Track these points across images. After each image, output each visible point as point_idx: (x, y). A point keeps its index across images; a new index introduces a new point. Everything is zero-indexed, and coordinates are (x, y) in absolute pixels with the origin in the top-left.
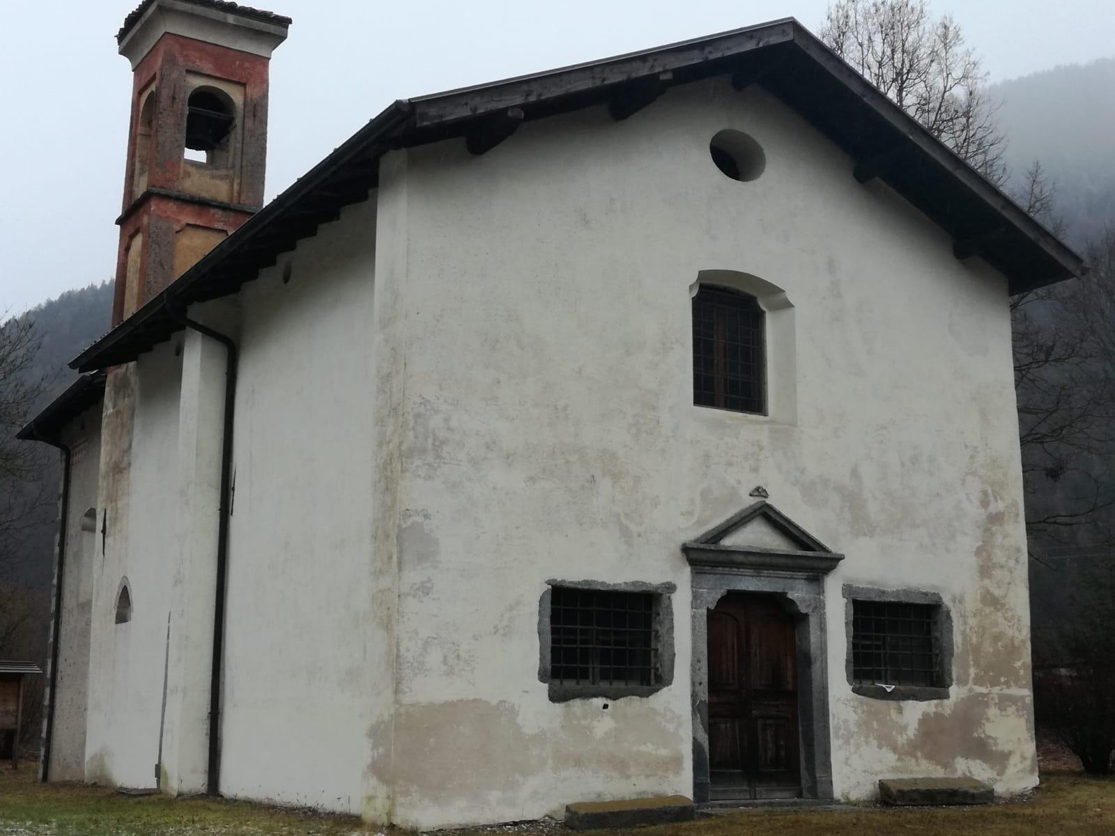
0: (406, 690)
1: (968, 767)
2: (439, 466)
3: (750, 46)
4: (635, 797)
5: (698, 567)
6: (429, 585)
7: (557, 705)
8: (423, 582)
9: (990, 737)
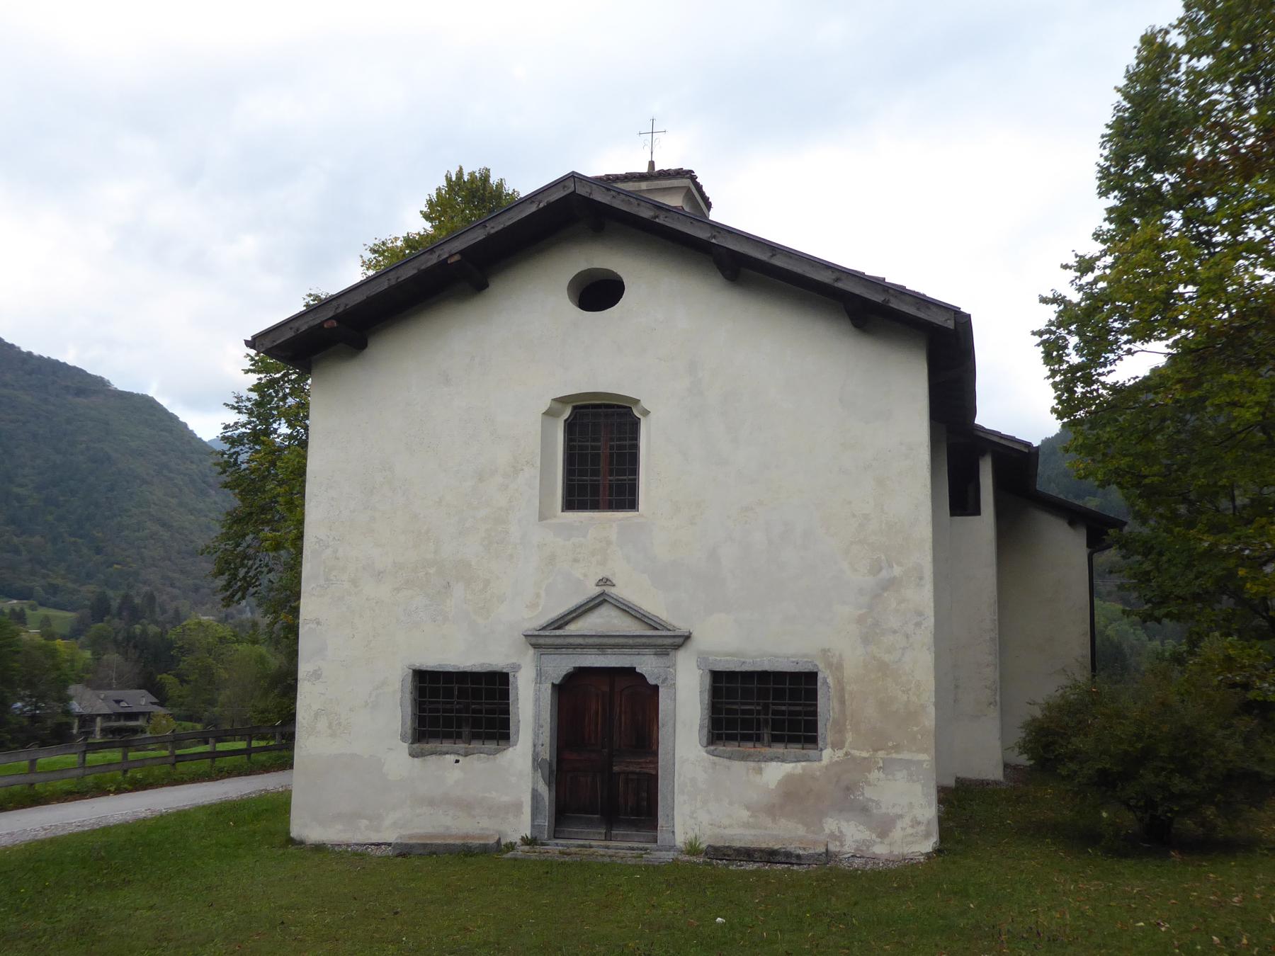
0: (303, 746)
1: (839, 828)
2: (328, 587)
3: (533, 208)
6: (320, 673)
8: (315, 670)
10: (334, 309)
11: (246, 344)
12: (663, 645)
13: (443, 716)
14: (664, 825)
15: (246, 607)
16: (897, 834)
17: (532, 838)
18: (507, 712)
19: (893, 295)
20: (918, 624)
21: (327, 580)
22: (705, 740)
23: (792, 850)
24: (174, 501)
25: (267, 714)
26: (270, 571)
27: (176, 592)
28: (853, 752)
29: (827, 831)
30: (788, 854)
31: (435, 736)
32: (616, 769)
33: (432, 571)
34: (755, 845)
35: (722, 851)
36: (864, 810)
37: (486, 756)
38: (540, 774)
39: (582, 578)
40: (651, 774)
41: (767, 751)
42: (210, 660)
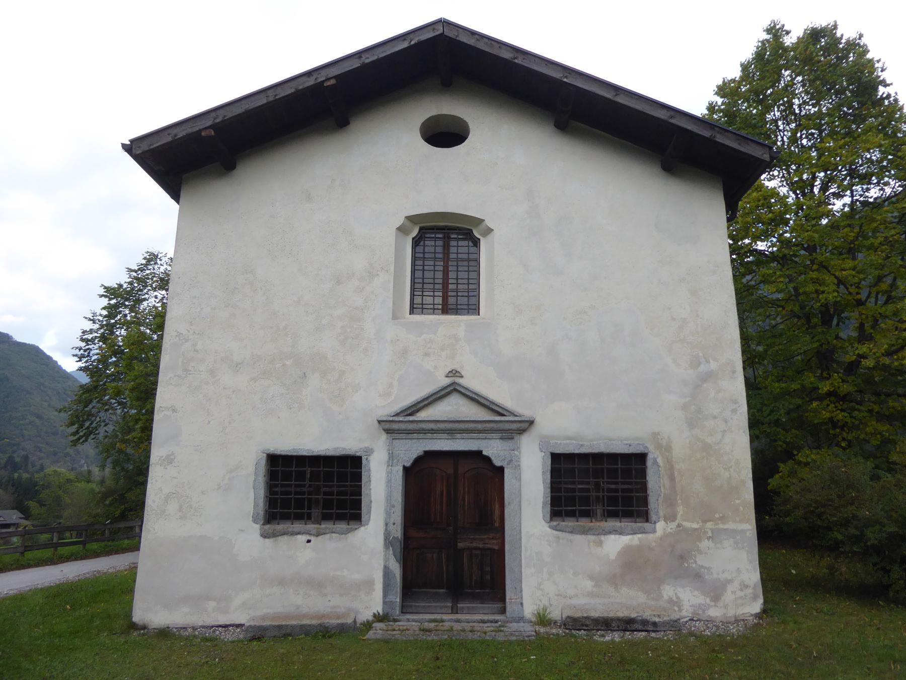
0: (151, 529)
1: (676, 594)
3: (405, 45)
4: (329, 610)
5: (393, 435)
6: (172, 457)
7: (267, 540)
9: (702, 567)
10: (212, 119)
11: (123, 148)
12: (509, 430)
13: (294, 498)
14: (512, 598)
15: (84, 463)
16: (728, 597)
17: (383, 614)
18: (360, 494)
19: (718, 132)
20: (734, 411)
21: (185, 370)
22: (548, 516)
23: (648, 618)
24: (46, 404)
25: (97, 518)
26: (106, 425)
27: (42, 455)
28: (685, 524)
29: (666, 597)
30: (645, 622)
31: (286, 517)
32: (460, 545)
33: (289, 362)
34: (611, 615)
35: (580, 621)
36: (696, 577)
37: (337, 535)
38: (391, 552)
39: (432, 370)
40: (494, 549)
41: (603, 524)
42: (61, 493)
